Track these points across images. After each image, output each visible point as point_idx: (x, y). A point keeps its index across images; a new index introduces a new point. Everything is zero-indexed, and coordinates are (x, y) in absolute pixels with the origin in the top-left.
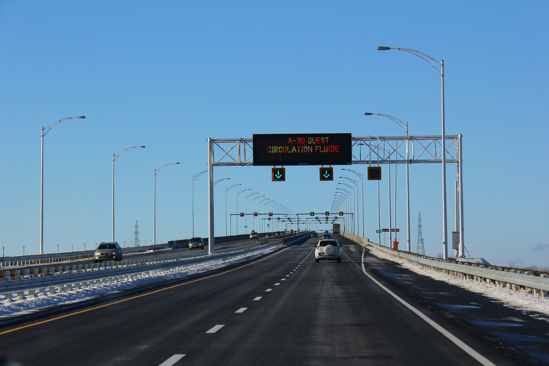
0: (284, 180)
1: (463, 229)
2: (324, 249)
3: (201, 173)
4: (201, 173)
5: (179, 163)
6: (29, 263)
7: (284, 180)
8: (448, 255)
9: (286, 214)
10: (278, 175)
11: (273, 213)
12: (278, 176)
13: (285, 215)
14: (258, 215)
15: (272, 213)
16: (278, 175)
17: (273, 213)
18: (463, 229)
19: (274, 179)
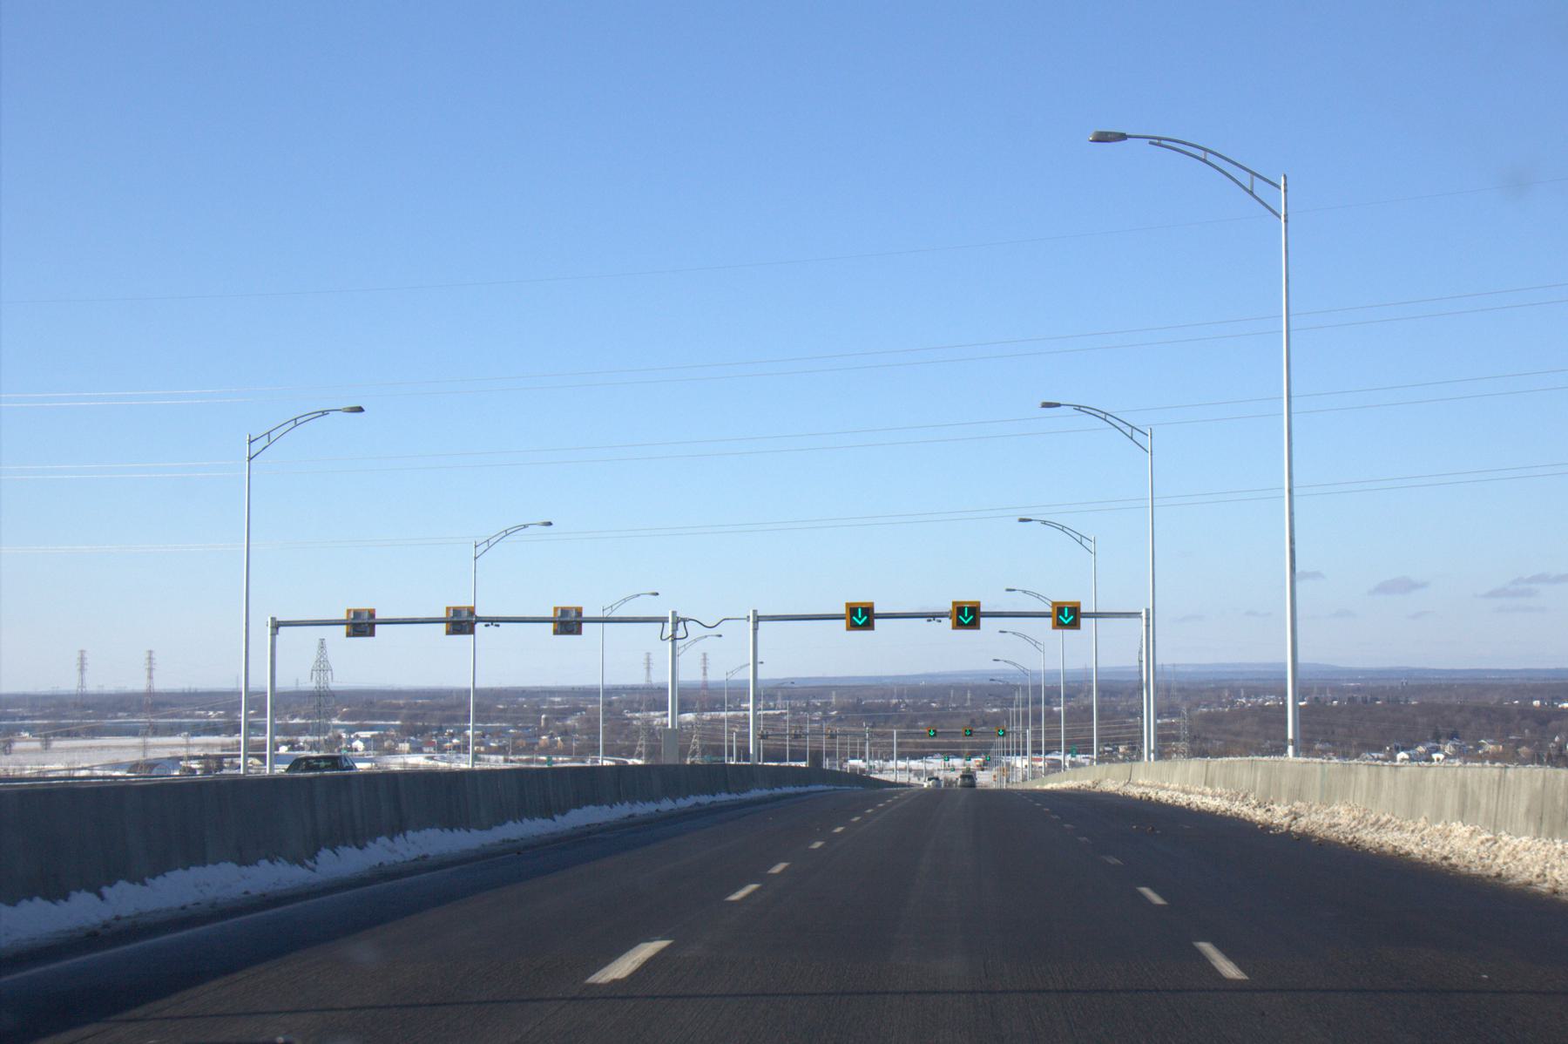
0: (1079, 628)
1: (1154, 641)
2: (931, 783)
3: (507, 533)
4: (507, 533)
5: (550, 524)
6: (860, 610)
7: (1079, 628)
8: (250, 686)
9: (676, 621)
10: (966, 615)
11: (378, 616)
12: (966, 619)
13: (669, 626)
14: (479, 627)
15: (471, 611)
16: (966, 615)
17: (479, 613)
18: (1154, 641)
19: (1058, 624)
